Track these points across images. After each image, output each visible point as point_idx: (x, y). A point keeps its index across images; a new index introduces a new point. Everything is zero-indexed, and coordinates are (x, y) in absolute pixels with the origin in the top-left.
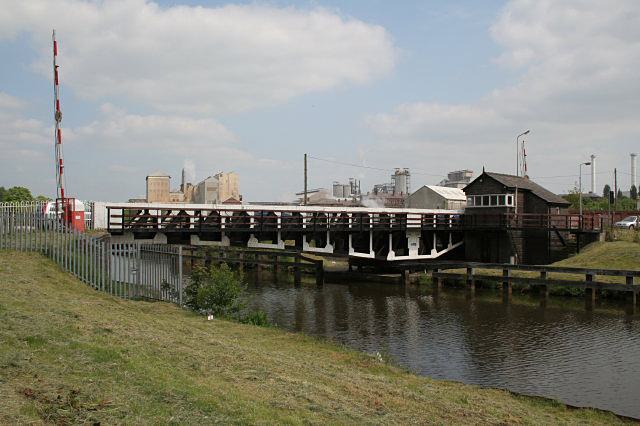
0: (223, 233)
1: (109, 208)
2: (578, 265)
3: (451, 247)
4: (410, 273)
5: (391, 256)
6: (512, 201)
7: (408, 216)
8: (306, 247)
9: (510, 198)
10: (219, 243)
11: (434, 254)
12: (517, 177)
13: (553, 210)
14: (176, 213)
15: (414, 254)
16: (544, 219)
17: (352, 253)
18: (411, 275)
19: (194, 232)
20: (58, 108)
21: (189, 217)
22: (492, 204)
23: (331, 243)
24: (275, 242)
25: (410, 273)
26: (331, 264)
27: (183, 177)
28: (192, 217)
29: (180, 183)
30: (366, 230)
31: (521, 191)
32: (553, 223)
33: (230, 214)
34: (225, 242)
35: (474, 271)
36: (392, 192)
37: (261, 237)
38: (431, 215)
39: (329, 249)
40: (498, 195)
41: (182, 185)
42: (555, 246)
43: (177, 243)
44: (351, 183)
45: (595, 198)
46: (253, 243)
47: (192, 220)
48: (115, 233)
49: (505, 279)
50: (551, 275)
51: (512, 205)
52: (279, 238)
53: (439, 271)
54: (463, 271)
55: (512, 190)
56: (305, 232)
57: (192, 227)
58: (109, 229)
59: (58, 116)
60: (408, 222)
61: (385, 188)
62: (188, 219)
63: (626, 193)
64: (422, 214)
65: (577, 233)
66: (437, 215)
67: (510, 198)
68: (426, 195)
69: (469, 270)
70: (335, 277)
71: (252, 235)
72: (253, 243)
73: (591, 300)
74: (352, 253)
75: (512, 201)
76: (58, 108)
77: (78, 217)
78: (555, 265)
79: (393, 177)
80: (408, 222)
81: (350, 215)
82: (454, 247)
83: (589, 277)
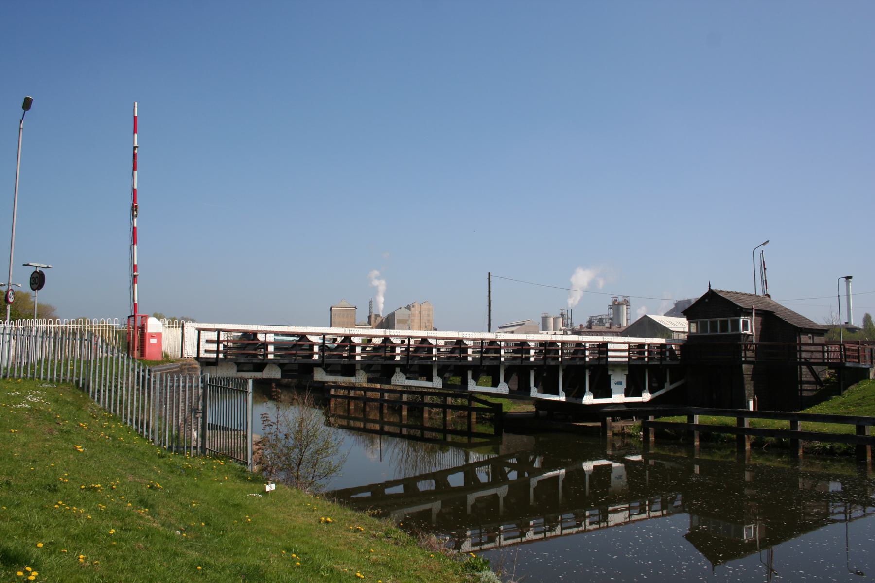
0: (358, 367)
1: (199, 331)
2: (841, 412)
3: (668, 387)
4: (613, 420)
5: (588, 399)
6: (749, 327)
7: (610, 346)
8: (472, 386)
9: (745, 323)
10: (352, 379)
11: (646, 397)
12: (755, 296)
13: (805, 339)
14: (377, 341)
15: (618, 398)
16: (793, 350)
17: (535, 393)
18: (614, 424)
19: (317, 364)
20: (134, 200)
21: (312, 345)
22: (722, 330)
23: (506, 381)
24: (430, 379)
25: (613, 420)
26: (512, 408)
27: (371, 307)
28: (398, 345)
29: (368, 315)
30: (553, 363)
31: (762, 313)
32: (804, 355)
33: (441, 343)
34: (360, 379)
35: (697, 419)
36: (608, 325)
37: (329, 369)
38: (641, 346)
39: (503, 388)
40: (729, 319)
41: (370, 317)
42: (808, 390)
43: (629, 370)
44: (562, 315)
45: (853, 330)
46: (399, 380)
47: (398, 350)
48: (207, 363)
49: (740, 430)
50: (802, 426)
51: (748, 332)
52: (435, 373)
53: (651, 418)
54: (684, 419)
55: (748, 312)
56: (470, 366)
57: (398, 358)
58: (198, 358)
59: (134, 208)
60: (610, 354)
61: (601, 320)
62: (393, 349)
63: (589, 395)
64: (629, 343)
65: (839, 367)
66: (649, 345)
67: (745, 323)
68: (647, 326)
69: (691, 419)
70: (517, 425)
71: (398, 370)
72: (399, 380)
73: (865, 464)
74: (535, 393)
75: (749, 327)
76: (134, 200)
77: (153, 341)
78: (810, 411)
79: (610, 307)
80: (610, 354)
81: (532, 344)
82: (672, 387)
83: (861, 429)
